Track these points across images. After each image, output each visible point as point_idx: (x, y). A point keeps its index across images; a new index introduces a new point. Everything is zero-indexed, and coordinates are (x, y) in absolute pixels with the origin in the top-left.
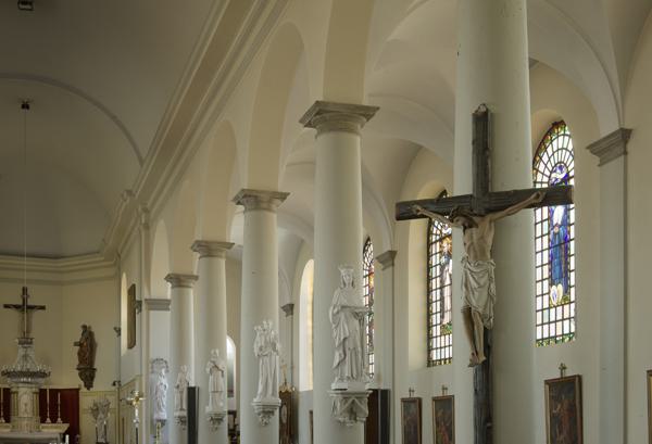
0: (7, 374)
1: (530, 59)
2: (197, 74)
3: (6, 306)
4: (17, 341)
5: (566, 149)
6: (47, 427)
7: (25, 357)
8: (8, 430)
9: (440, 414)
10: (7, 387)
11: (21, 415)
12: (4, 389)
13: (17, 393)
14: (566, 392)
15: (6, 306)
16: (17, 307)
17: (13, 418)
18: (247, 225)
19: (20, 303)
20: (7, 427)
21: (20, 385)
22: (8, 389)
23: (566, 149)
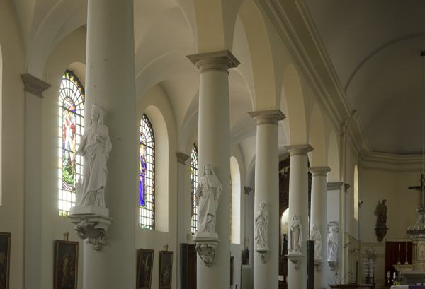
0: (410, 232)
1: (85, 64)
2: (319, 54)
3: (410, 188)
4: (417, 210)
5: (67, 88)
6: (404, 268)
7: (422, 220)
8: (410, 269)
9: (167, 272)
10: (410, 240)
11: (419, 259)
12: (408, 242)
13: (417, 244)
14: (65, 254)
15: (410, 188)
16: (417, 188)
17: (413, 261)
18: (58, 206)
19: (420, 185)
20: (410, 267)
21: (419, 239)
22: (411, 242)
23: (67, 88)
